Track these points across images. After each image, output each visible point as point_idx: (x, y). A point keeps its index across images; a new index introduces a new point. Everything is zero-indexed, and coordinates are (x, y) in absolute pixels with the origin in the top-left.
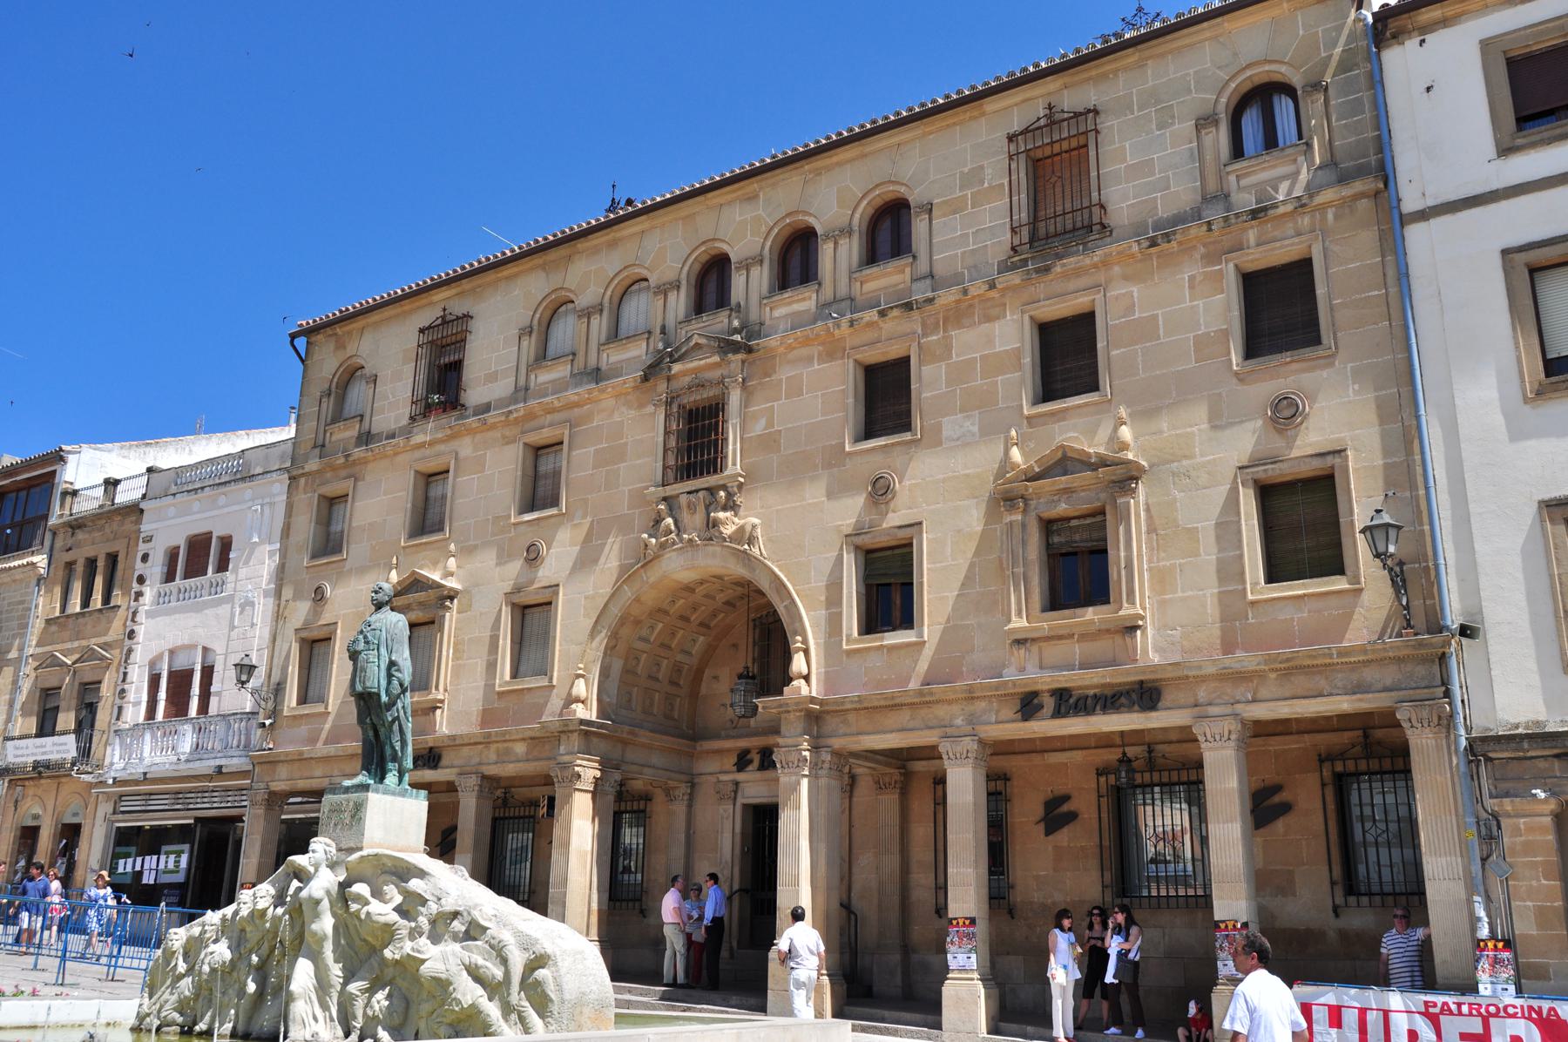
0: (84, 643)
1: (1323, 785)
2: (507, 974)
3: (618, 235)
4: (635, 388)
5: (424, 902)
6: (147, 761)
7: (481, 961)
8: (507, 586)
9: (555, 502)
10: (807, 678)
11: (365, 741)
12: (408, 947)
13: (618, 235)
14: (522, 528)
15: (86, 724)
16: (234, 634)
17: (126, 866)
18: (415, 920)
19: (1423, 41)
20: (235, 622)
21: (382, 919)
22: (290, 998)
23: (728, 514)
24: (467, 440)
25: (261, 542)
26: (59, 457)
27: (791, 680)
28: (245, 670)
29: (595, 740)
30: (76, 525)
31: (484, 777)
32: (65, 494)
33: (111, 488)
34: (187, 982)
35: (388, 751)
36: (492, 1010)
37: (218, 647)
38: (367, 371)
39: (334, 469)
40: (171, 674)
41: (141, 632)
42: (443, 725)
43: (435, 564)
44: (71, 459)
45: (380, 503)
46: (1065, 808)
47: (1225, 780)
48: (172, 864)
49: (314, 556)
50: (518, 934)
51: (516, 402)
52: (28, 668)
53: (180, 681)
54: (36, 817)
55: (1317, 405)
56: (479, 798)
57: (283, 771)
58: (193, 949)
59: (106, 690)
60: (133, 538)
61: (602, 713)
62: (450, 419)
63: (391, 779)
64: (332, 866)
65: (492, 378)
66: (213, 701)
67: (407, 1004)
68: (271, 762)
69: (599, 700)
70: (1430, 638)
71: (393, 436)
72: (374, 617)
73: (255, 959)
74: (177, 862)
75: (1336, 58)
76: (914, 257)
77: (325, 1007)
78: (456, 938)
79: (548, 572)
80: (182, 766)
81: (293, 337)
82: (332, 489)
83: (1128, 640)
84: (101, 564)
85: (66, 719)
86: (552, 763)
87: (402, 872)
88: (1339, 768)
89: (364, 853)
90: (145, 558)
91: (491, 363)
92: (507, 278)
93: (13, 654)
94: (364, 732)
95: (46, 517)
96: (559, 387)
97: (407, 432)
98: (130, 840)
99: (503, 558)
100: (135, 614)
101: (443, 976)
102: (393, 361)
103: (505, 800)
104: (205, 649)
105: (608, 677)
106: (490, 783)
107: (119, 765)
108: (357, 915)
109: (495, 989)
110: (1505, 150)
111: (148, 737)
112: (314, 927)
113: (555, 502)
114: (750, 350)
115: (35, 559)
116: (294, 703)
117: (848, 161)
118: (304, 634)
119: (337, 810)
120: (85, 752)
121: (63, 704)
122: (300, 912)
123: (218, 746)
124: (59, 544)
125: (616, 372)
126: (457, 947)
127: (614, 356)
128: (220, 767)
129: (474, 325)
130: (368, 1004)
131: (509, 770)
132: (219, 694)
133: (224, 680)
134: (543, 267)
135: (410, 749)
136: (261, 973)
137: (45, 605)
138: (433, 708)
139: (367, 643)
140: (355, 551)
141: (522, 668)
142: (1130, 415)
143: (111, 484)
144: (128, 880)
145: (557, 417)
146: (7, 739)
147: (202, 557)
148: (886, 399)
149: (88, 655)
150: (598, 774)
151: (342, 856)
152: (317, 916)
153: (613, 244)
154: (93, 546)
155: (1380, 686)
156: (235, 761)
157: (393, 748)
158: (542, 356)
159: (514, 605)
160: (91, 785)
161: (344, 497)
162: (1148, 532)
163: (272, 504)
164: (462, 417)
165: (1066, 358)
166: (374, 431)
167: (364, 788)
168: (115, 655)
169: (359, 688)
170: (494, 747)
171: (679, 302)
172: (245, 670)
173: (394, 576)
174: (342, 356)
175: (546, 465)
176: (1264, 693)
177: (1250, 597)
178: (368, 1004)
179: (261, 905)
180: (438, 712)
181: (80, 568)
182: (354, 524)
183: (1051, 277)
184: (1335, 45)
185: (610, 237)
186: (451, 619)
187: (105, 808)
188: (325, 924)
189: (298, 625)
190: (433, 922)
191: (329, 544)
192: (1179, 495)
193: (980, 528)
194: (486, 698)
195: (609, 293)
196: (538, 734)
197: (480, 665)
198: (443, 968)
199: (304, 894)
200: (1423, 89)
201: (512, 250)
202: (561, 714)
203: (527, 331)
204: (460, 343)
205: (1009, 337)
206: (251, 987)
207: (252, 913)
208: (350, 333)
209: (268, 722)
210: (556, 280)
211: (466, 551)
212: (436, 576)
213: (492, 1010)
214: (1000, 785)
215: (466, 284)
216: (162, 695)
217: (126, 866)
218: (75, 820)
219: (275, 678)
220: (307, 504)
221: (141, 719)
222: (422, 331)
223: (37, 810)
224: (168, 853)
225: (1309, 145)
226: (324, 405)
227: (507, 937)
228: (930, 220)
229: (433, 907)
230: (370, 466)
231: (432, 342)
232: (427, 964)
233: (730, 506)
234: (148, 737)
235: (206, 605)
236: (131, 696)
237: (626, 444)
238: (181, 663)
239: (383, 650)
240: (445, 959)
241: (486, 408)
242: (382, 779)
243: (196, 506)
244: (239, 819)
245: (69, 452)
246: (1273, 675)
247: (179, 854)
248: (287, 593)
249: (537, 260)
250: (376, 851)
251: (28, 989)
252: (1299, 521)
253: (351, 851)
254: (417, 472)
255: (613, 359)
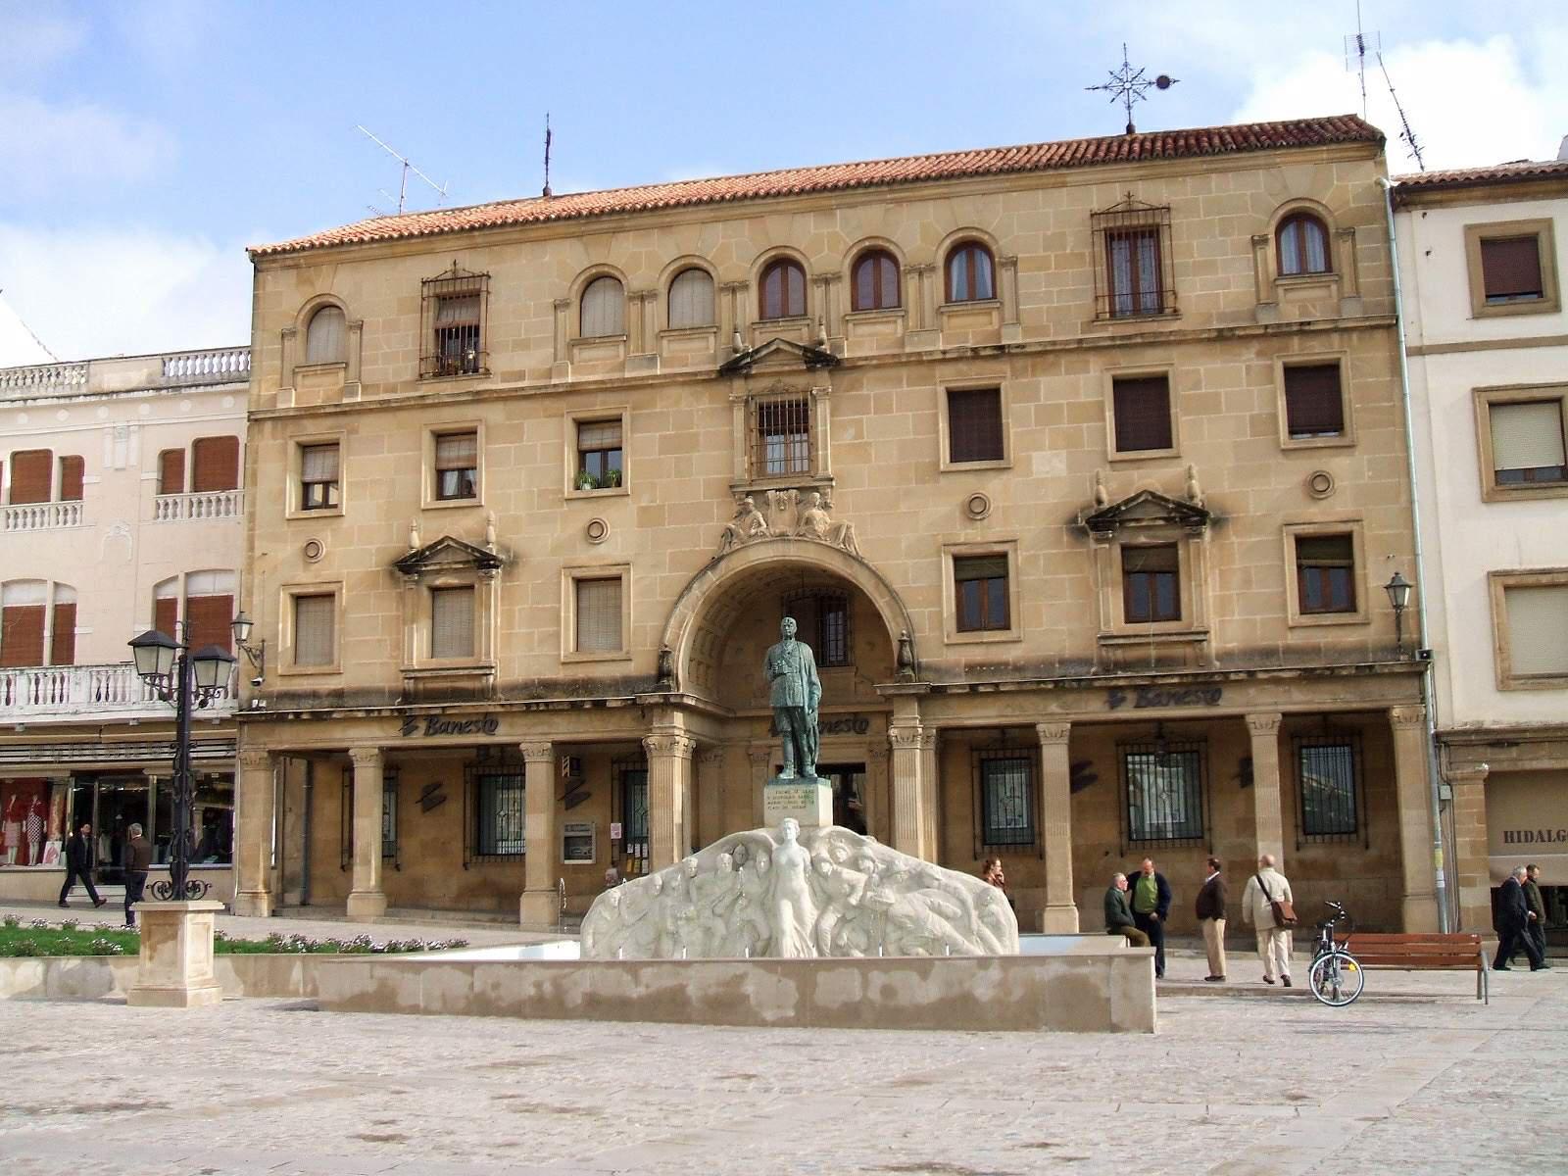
1: (613, 779)
19: (1425, 214)
46: (1087, 772)
47: (1055, 760)
70: (1413, 662)
76: (1001, 303)
88: (984, 755)
110: (1477, 316)
148: (976, 426)
165: (1143, 413)
171: (748, 304)
200: (1432, 253)
205: (1089, 386)
214: (393, 773)
228: (1016, 272)
237: (696, 435)
252: (1326, 563)
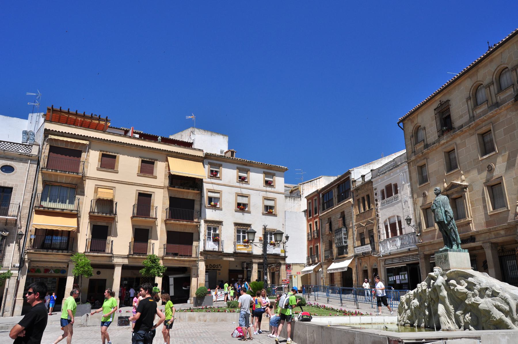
0: (367, 220)
2: (510, 308)
3: (492, 57)
4: (513, 105)
5: (475, 285)
6: (390, 249)
7: (499, 304)
8: (484, 180)
9: (493, 150)
11: (444, 236)
12: (473, 300)
13: (492, 57)
14: (483, 161)
15: (372, 241)
16: (404, 210)
17: (391, 279)
18: (473, 291)
20: (404, 207)
21: (462, 291)
22: (439, 316)
24: (458, 138)
25: (405, 183)
26: (349, 173)
28: (409, 220)
30: (357, 189)
31: (492, 243)
32: (353, 182)
34: (408, 311)
35: (452, 239)
36: (508, 320)
37: (401, 215)
38: (422, 127)
39: (419, 157)
40: (390, 225)
41: (380, 214)
42: (473, 228)
43: (457, 179)
44: (352, 172)
45: (436, 164)
48: (402, 278)
49: (420, 184)
50: (511, 294)
51: (471, 122)
52: (355, 229)
53: (393, 226)
54: (366, 267)
56: (492, 250)
57: (427, 248)
58: (408, 301)
59: (375, 231)
60: (372, 189)
62: (451, 134)
63: (455, 247)
64: (442, 275)
65: (461, 117)
66: (403, 230)
67: (478, 318)
68: (422, 246)
71: (434, 143)
72: (437, 198)
73: (426, 304)
74: (405, 277)
77: (451, 319)
78: (489, 296)
79: (497, 173)
80: (399, 250)
81: (398, 123)
82: (421, 163)
84: (365, 198)
85: (367, 241)
86: (515, 236)
87: (466, 276)
89: (451, 270)
90: (376, 194)
91: (459, 111)
92: (458, 85)
93: (351, 226)
94: (442, 233)
95: (350, 189)
96: (484, 113)
97: (438, 141)
98: (391, 272)
99: (480, 172)
100: (377, 210)
101: (487, 309)
102: (429, 120)
103: (503, 250)
104: (398, 216)
106: (494, 245)
107: (383, 251)
108: (453, 290)
109: (508, 313)
111: (388, 243)
112: (441, 294)
113: (493, 150)
115: (350, 200)
116: (425, 228)
118: (423, 207)
119: (440, 258)
120: (374, 249)
121: (365, 237)
122: (436, 290)
123: (407, 243)
124: (354, 195)
125: (504, 101)
126: (490, 299)
127: (502, 97)
128: (409, 249)
129: (451, 103)
130: (464, 318)
131: (500, 240)
132: (404, 228)
133: (404, 224)
134: (469, 77)
135: (458, 237)
136: (429, 308)
137: (355, 211)
138: (468, 223)
139: (436, 206)
140: (432, 180)
141: (496, 206)
143: (363, 177)
144: (393, 283)
145: (487, 122)
146: (354, 247)
147: (391, 191)
149: (368, 223)
151: (444, 272)
152: (441, 291)
153: (491, 61)
154: (362, 194)
156: (413, 247)
157: (453, 237)
158: (476, 105)
159: (488, 187)
160: (377, 258)
161: (424, 165)
163: (405, 172)
164: (455, 132)
166: (428, 143)
167: (446, 250)
168: (375, 222)
169: (437, 220)
170: (493, 233)
173: (446, 185)
174: (413, 124)
175: (487, 139)
178: (464, 318)
179: (424, 288)
180: (471, 224)
181: (361, 200)
182: (430, 172)
185: (490, 58)
186: (467, 195)
187: (382, 264)
188: (444, 293)
189: (421, 205)
190: (480, 291)
191: (424, 179)
194: (486, 218)
195: (494, 77)
196: (508, 227)
197: (481, 207)
198: (486, 306)
199: (435, 284)
201: (457, 76)
202: (514, 219)
203: (469, 99)
204: (448, 109)
206: (427, 313)
207: (422, 290)
208: (414, 117)
209: (419, 234)
210: (474, 79)
211: (467, 172)
212: (459, 182)
213: (508, 320)
215: (445, 91)
216: (389, 231)
217: (391, 279)
218: (376, 267)
219: (418, 221)
220: (414, 168)
221: (386, 238)
222: (435, 110)
223: (366, 265)
224: (401, 275)
226: (412, 140)
227: (507, 296)
229: (478, 287)
230: (430, 154)
231: (439, 112)
232: (481, 305)
234: (388, 243)
235: (395, 204)
236: (382, 232)
238: (392, 221)
239: (442, 208)
240: (486, 303)
241: (462, 126)
242: (452, 247)
243: (385, 177)
244: (418, 263)
247: (404, 275)
248: (415, 196)
249: (466, 75)
250: (455, 270)
251: (369, 313)
253: (447, 270)
254: (445, 152)
255: (502, 98)
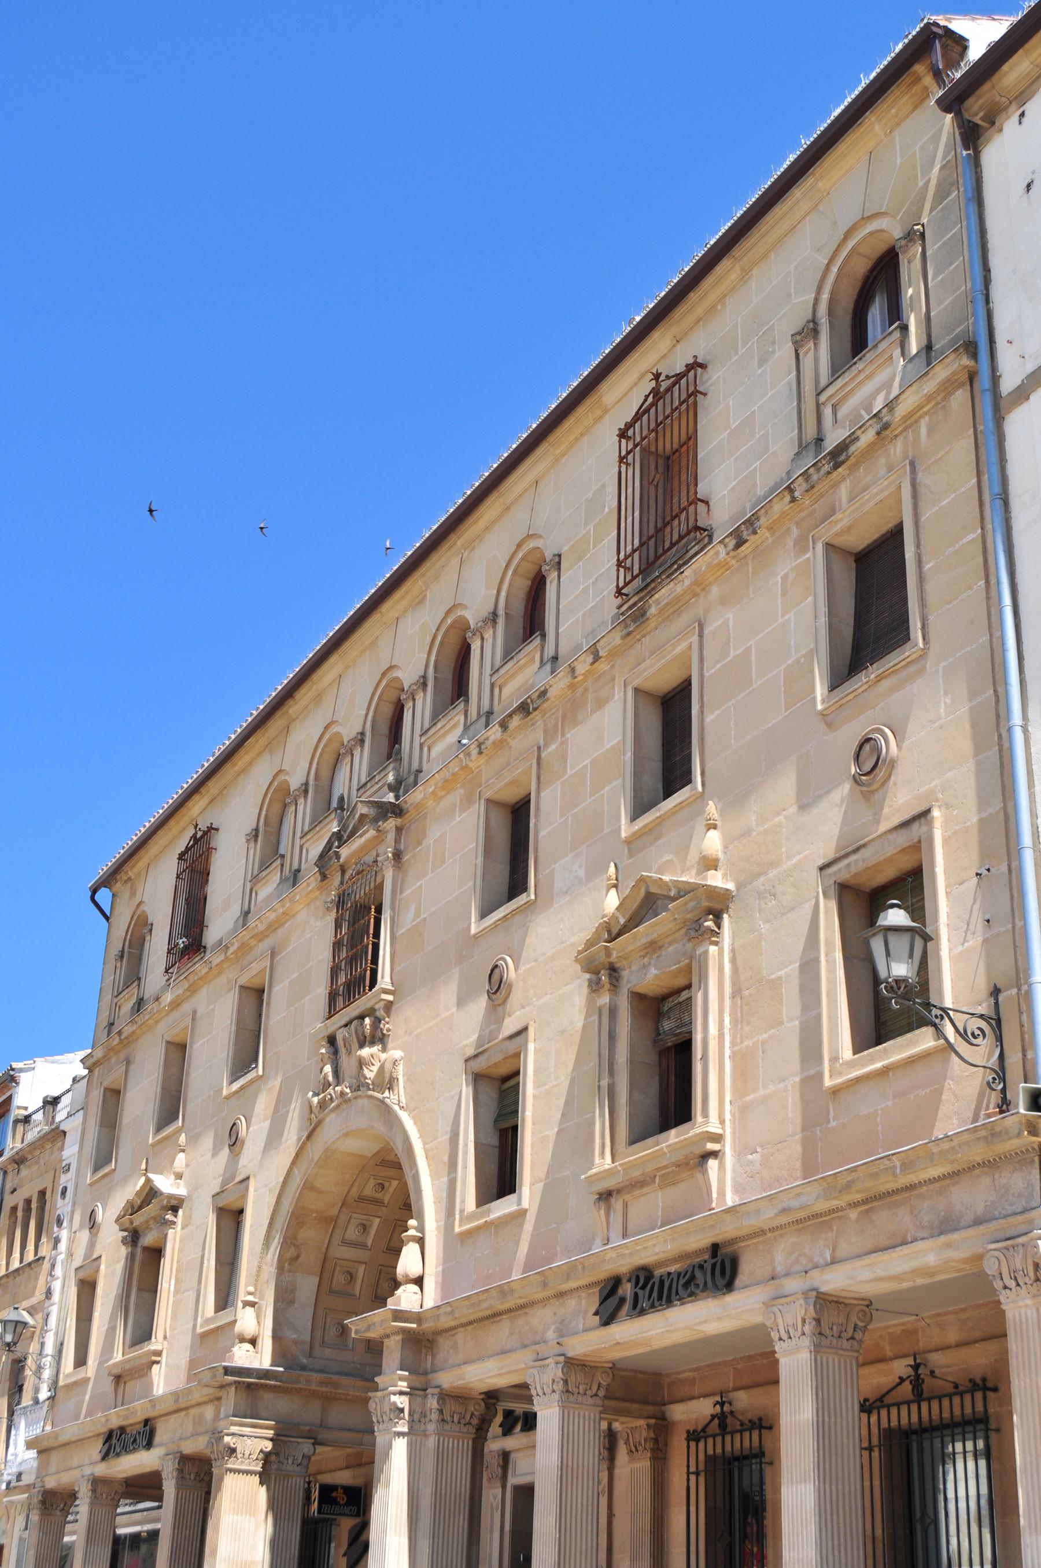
10: (419, 1281)
19: (1022, 115)
23: (375, 1049)
27: (396, 1284)
29: (267, 1396)
33: (50, 1108)
44: (24, 1078)
55: (907, 743)
61: (280, 1353)
69: (276, 1337)
75: (933, 182)
83: (699, 1176)
105: (291, 1302)
114: (397, 811)
117: (496, 521)
142: (721, 812)
150: (268, 1446)
155: (969, 1217)
162: (733, 997)
172: (10, 1327)
176: (844, 1248)
177: (828, 1082)
183: (653, 623)
184: (932, 165)
192: (764, 928)
193: (580, 1024)
203: (255, 834)
215: (213, 786)
225: (904, 328)
233: (378, 1038)
245: (21, 1070)
246: (853, 1215)
